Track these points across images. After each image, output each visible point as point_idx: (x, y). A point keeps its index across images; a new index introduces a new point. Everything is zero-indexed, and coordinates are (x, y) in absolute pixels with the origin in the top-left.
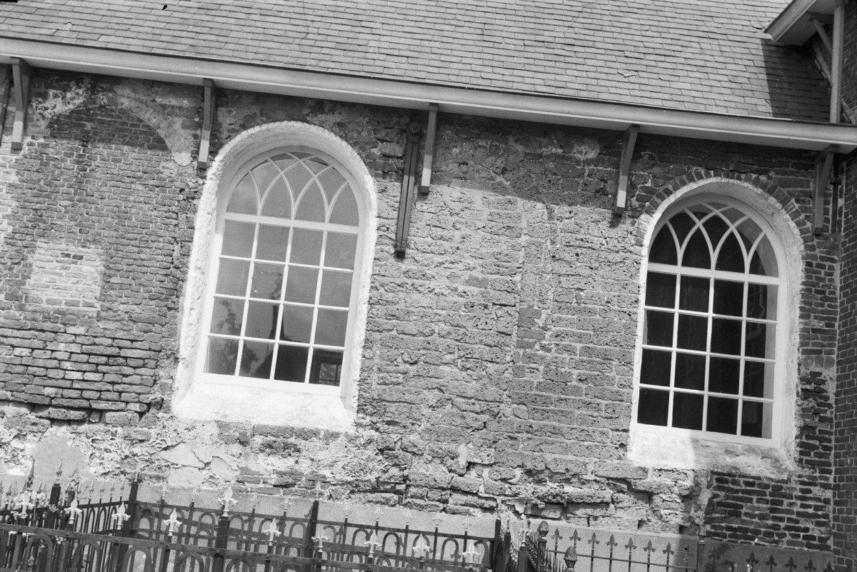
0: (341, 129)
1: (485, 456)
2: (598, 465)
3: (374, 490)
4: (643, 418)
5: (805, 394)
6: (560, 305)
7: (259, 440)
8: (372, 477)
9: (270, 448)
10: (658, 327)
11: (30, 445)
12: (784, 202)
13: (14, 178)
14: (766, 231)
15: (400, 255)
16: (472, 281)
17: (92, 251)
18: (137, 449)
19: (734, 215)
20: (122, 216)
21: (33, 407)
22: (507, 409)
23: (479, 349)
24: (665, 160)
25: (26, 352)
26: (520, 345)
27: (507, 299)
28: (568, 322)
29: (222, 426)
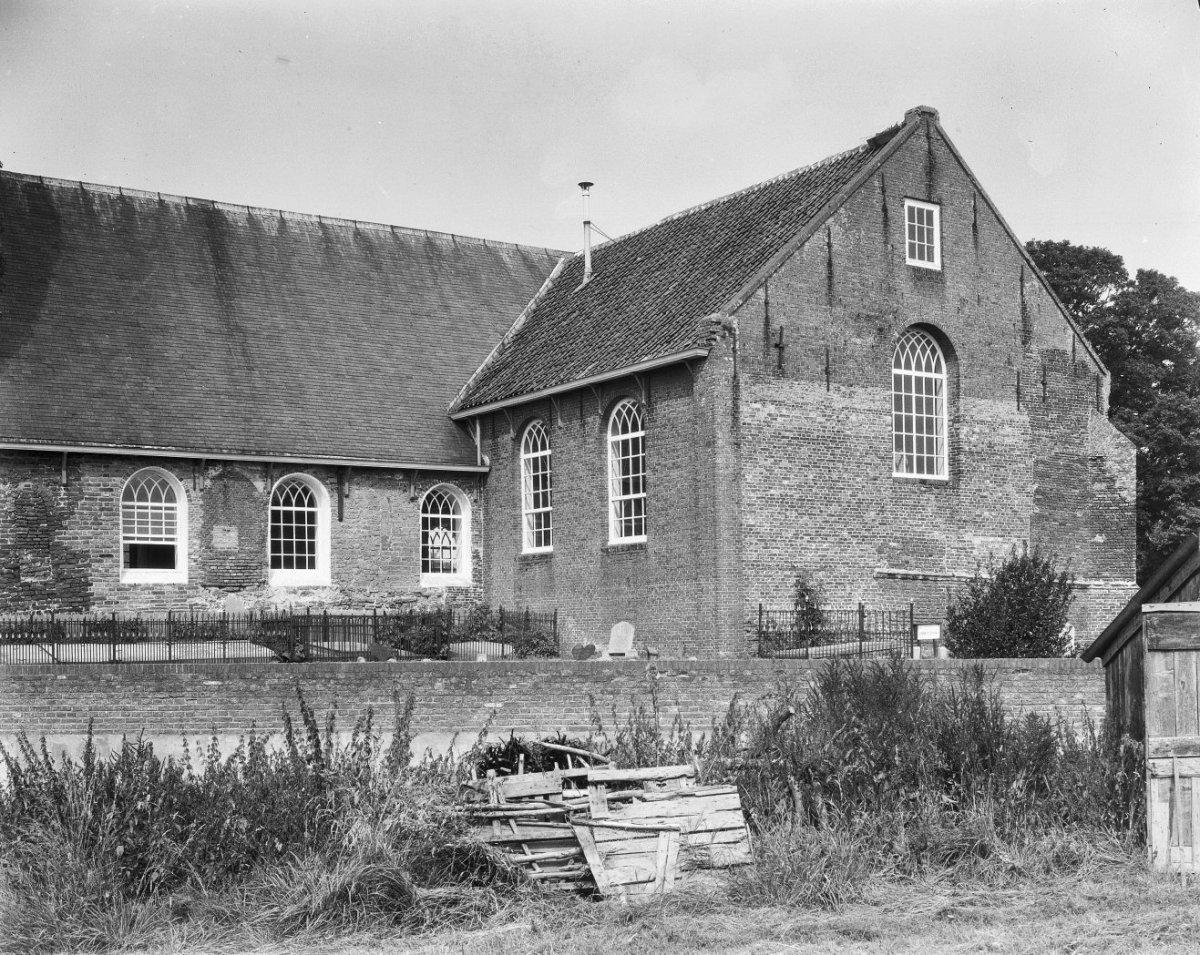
0: (315, 474)
1: (376, 589)
2: (410, 588)
3: (341, 605)
4: (423, 571)
5: (474, 557)
6: (395, 534)
7: (301, 591)
8: (340, 601)
9: (304, 594)
10: (275, 532)
11: (222, 601)
12: (464, 490)
13: (201, 502)
14: (457, 498)
15: (341, 520)
16: (365, 528)
17: (233, 528)
18: (260, 599)
19: (446, 493)
20: (242, 514)
21: (220, 587)
22: (381, 572)
23: (369, 552)
24: (425, 478)
25: (215, 568)
26: (383, 549)
27: (376, 533)
28: (397, 540)
29: (287, 588)
